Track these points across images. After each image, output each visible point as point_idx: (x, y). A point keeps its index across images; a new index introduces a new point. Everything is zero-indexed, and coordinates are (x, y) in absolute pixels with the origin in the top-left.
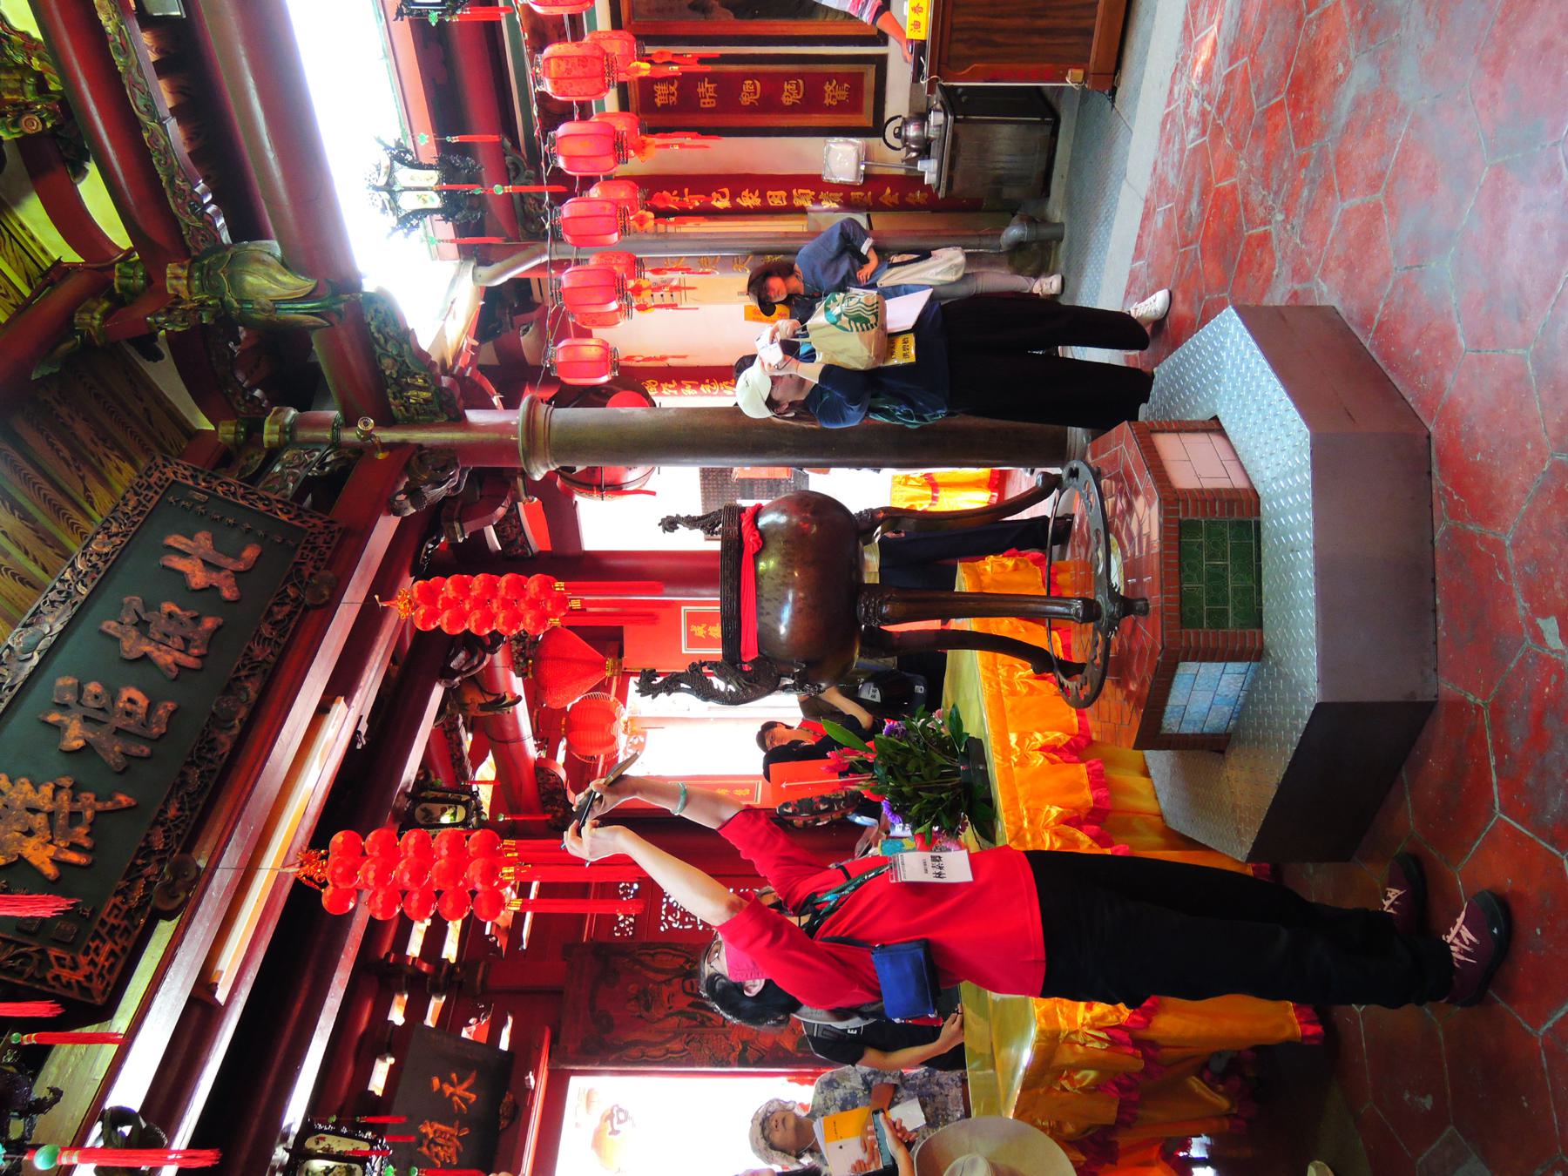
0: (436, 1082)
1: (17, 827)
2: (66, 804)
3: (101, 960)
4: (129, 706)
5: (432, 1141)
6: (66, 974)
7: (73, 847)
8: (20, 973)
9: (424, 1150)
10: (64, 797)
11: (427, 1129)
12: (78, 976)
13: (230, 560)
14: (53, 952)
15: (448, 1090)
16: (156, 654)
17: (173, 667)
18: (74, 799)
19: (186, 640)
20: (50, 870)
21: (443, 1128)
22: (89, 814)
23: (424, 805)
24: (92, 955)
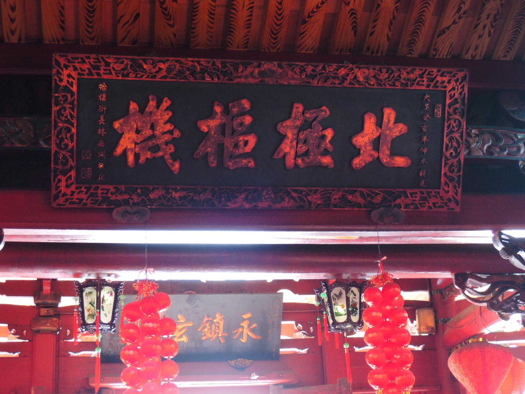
0: (248, 316)
1: (139, 124)
2: (162, 140)
3: (76, 196)
4: (241, 143)
5: (212, 321)
6: (63, 184)
7: (137, 156)
8: (56, 163)
10: (167, 137)
11: (218, 318)
12: (63, 189)
13: (387, 152)
14: (73, 173)
15: (245, 324)
16: (288, 141)
17: (281, 154)
18: (167, 144)
19: (306, 153)
21: (221, 327)
23: (344, 292)
24: (77, 191)
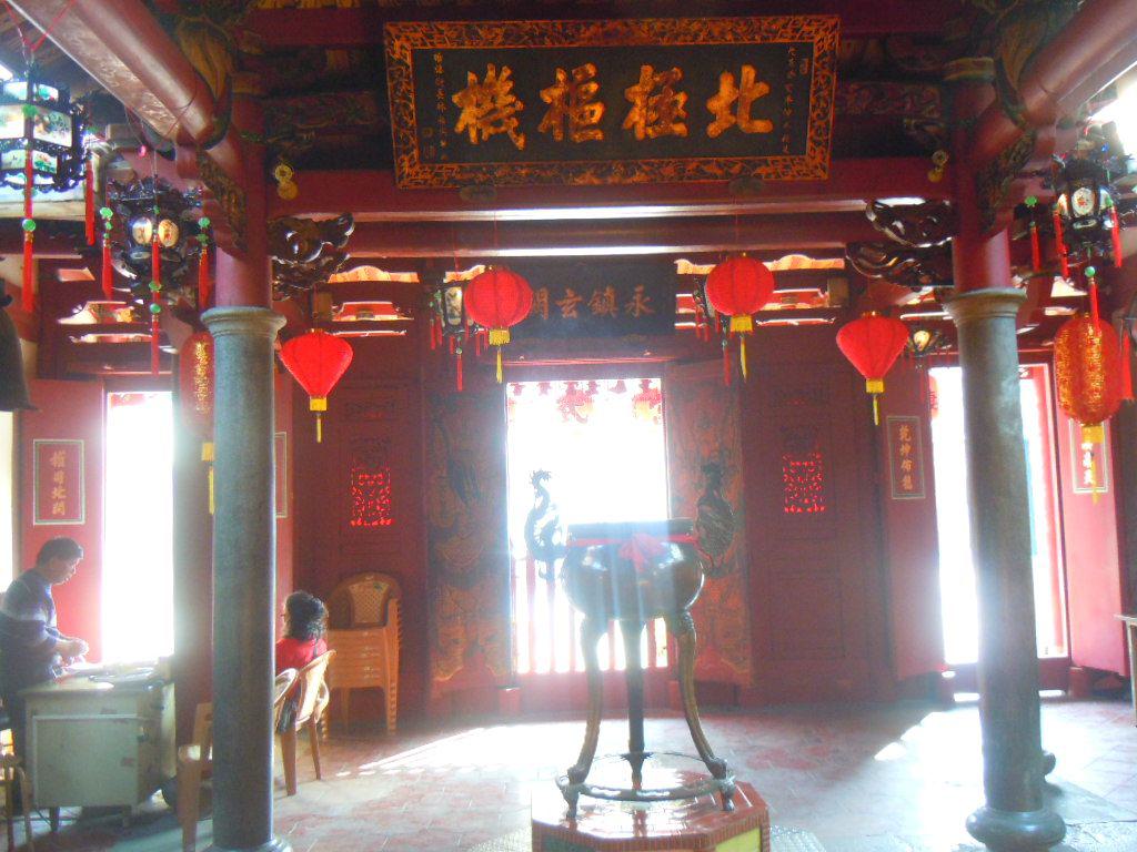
2: (505, 114)
5: (603, 297)
6: (406, 164)
7: (479, 132)
9: (596, 293)
10: (508, 111)
15: (637, 297)
20: (460, 127)
22: (503, 129)
